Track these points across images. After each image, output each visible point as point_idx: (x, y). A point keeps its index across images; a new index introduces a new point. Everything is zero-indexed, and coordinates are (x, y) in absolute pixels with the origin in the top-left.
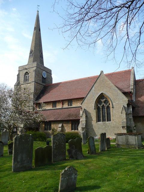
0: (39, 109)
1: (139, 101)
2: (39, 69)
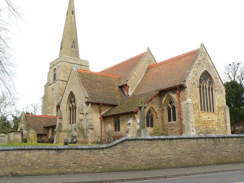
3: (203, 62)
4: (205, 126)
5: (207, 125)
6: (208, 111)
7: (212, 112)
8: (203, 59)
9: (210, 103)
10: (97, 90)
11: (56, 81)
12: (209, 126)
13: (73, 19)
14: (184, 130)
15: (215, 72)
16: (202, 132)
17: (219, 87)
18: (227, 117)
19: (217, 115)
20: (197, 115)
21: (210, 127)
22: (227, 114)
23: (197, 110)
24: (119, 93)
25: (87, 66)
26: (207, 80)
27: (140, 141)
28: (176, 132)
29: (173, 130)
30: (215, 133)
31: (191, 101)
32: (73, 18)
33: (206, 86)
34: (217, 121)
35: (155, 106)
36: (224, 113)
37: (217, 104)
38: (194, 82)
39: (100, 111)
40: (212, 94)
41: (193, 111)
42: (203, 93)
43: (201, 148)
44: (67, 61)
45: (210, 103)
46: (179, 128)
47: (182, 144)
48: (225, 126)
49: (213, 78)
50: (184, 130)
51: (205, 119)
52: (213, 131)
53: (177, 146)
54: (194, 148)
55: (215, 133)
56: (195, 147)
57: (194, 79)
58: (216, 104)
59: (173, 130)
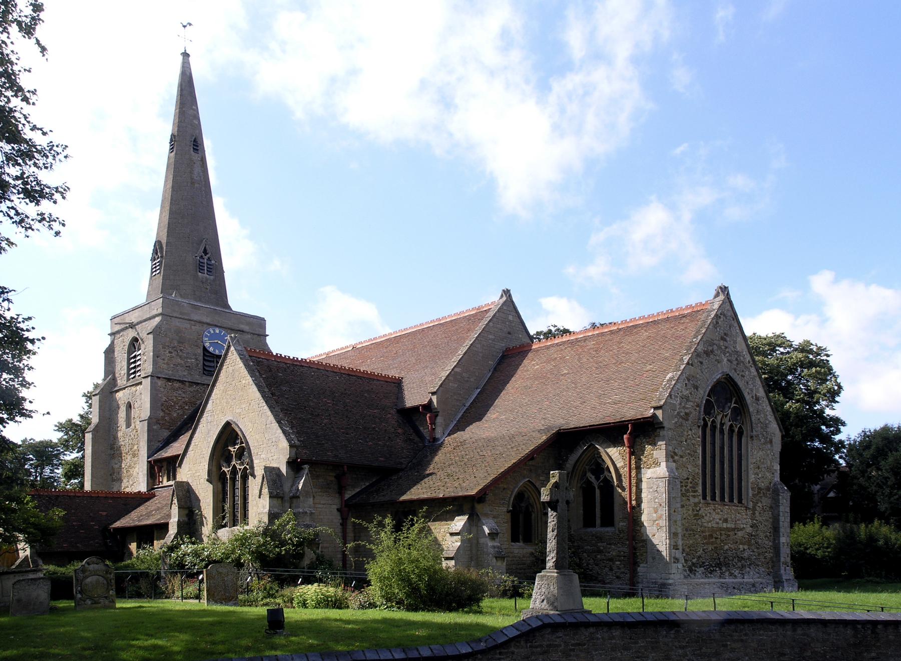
0: (168, 480)
1: (674, 547)
2: (177, 323)
3: (719, 347)
4: (712, 543)
5: (718, 541)
6: (722, 498)
7: (735, 501)
8: (723, 339)
9: (731, 474)
10: (325, 421)
11: (143, 380)
12: (726, 544)
13: (197, 169)
14: (642, 555)
15: (753, 378)
16: (703, 563)
17: (762, 428)
18: (782, 519)
19: (750, 512)
20: (690, 512)
21: (726, 547)
22: (782, 508)
23: (691, 498)
24: (400, 431)
25: (259, 335)
26: (726, 403)
27: (592, 630)
28: (611, 560)
29: (600, 552)
30: (739, 564)
31: (675, 470)
32: (199, 163)
33: (722, 424)
34: (749, 530)
35: (541, 478)
36: (775, 504)
37: (752, 478)
38: (687, 411)
39: (341, 491)
40: (740, 448)
41: (679, 500)
42: (713, 444)
43: (809, 654)
44: (181, 313)
45: (731, 474)
46: (626, 550)
47: (742, 641)
48: (771, 544)
49: (748, 398)
50: (642, 555)
51: (715, 525)
52: (736, 560)
53: (725, 646)
54: (785, 655)
55: (739, 564)
56: (787, 651)
57: (688, 400)
58: (752, 478)
59: (600, 552)
